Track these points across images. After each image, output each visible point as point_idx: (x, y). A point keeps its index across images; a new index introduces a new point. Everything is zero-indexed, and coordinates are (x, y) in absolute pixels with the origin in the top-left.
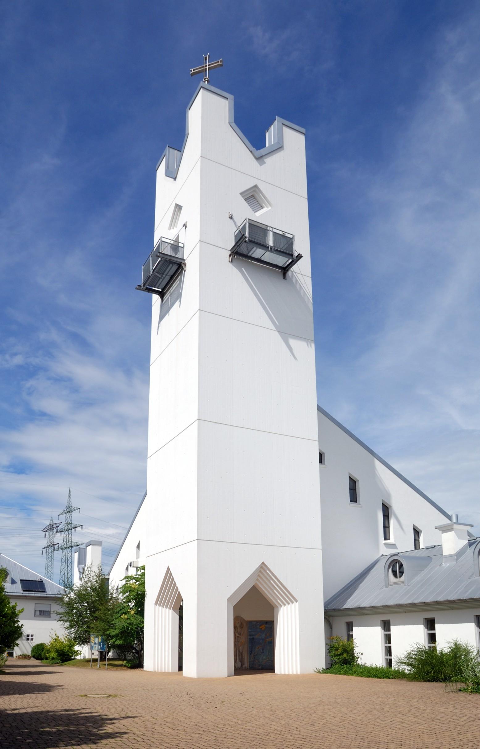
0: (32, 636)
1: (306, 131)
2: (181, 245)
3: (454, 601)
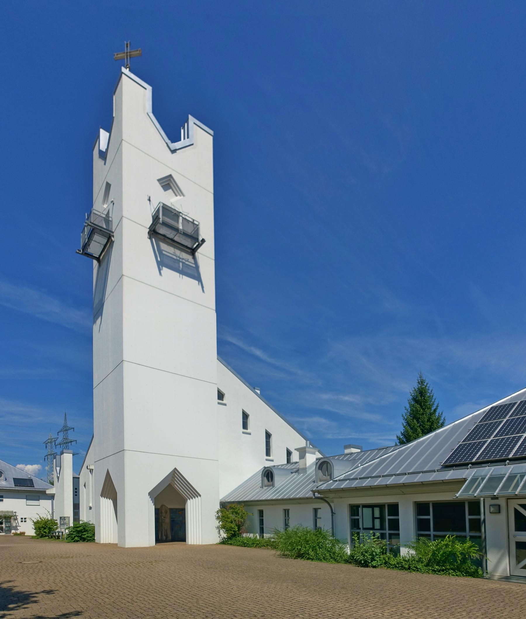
0: (25, 519)
1: (214, 133)
2: (110, 219)
3: (300, 499)
